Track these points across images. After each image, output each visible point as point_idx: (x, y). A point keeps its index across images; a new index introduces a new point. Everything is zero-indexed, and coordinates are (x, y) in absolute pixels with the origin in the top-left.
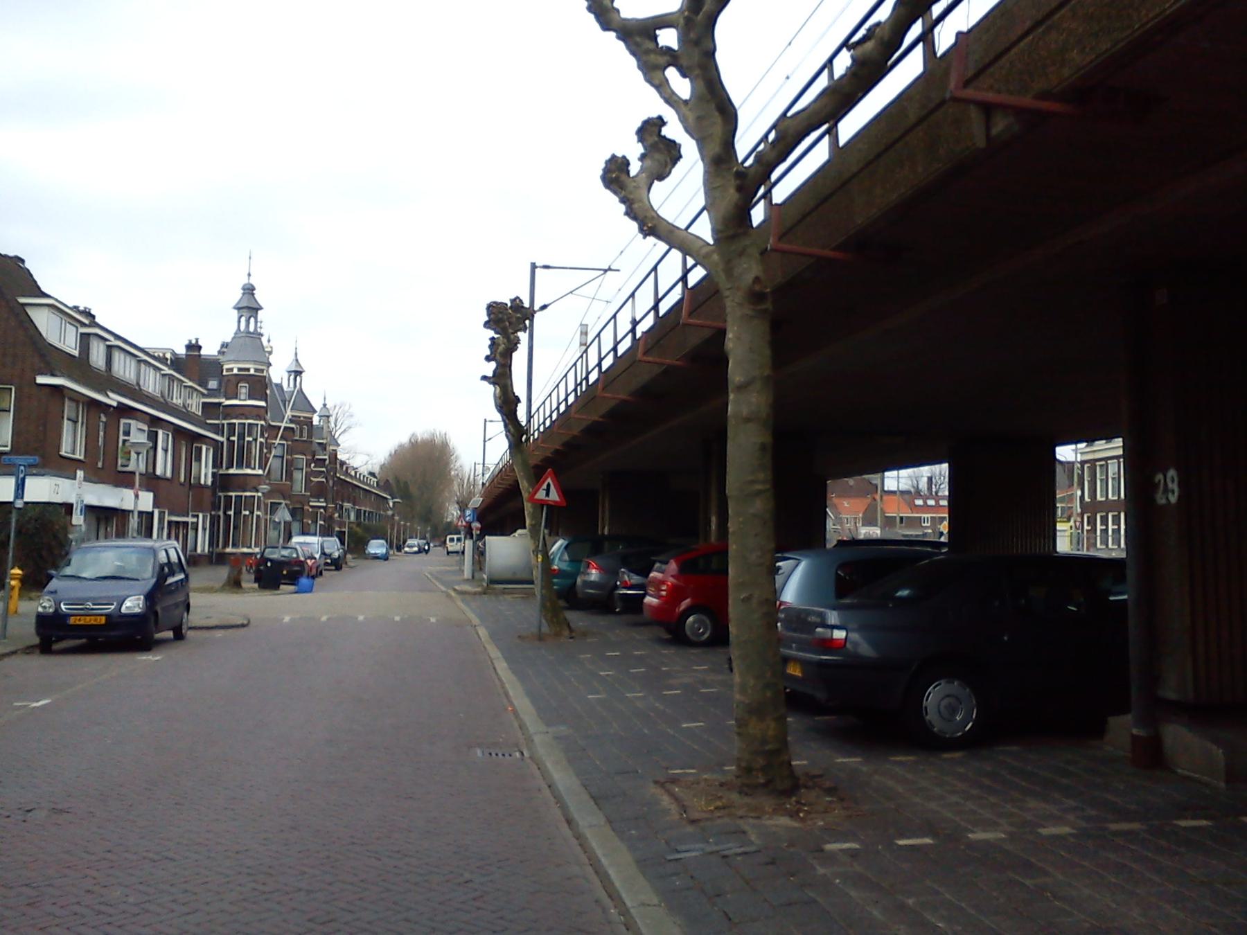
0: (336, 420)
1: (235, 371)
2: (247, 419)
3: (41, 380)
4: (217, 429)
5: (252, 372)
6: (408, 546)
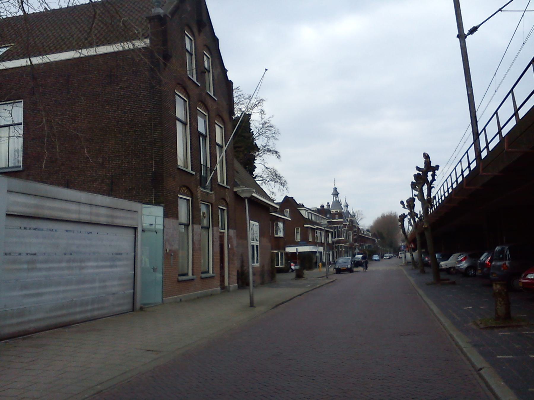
0: (357, 216)
1: (334, 212)
2: (339, 224)
3: (305, 226)
4: (331, 228)
5: (339, 212)
6: (385, 257)
